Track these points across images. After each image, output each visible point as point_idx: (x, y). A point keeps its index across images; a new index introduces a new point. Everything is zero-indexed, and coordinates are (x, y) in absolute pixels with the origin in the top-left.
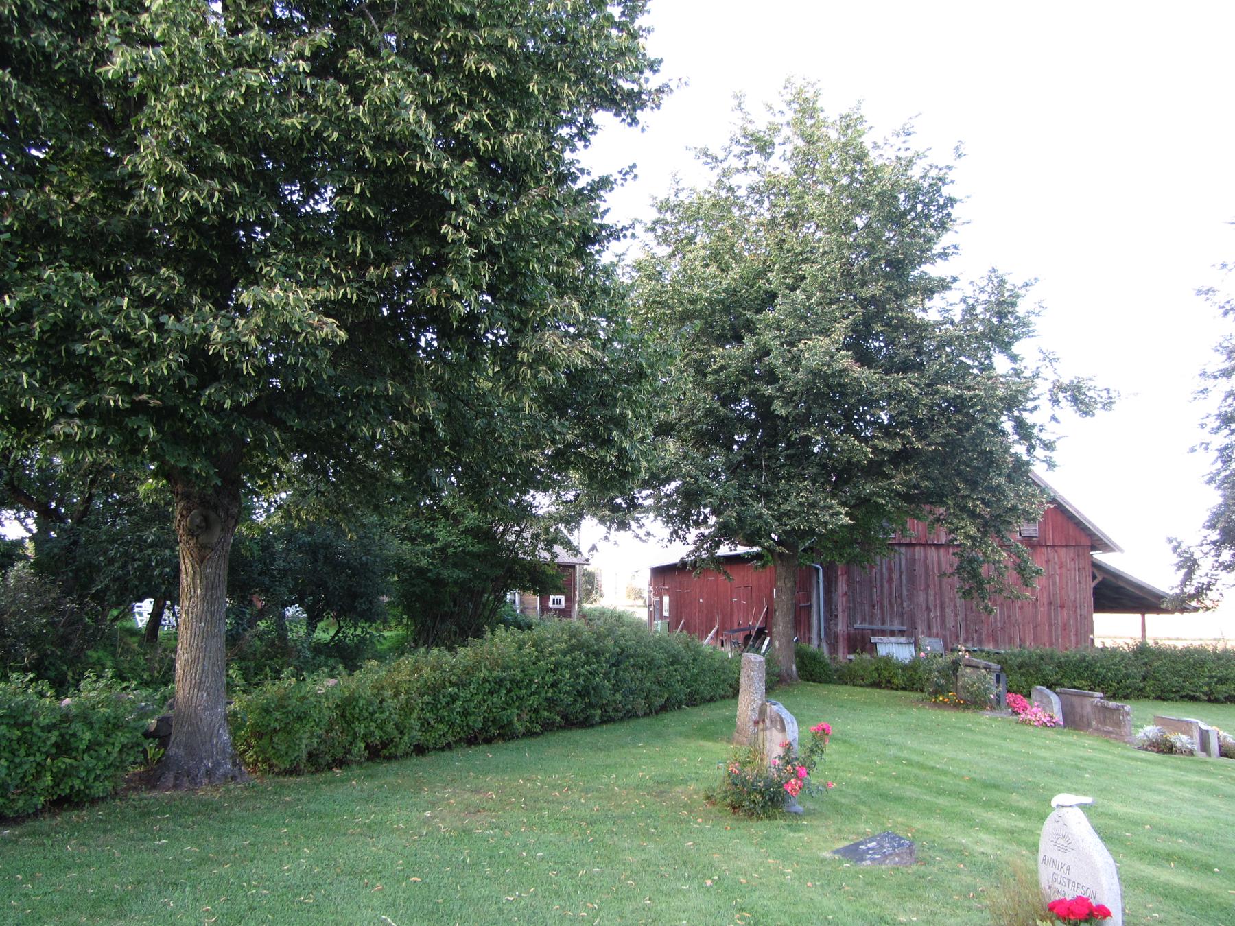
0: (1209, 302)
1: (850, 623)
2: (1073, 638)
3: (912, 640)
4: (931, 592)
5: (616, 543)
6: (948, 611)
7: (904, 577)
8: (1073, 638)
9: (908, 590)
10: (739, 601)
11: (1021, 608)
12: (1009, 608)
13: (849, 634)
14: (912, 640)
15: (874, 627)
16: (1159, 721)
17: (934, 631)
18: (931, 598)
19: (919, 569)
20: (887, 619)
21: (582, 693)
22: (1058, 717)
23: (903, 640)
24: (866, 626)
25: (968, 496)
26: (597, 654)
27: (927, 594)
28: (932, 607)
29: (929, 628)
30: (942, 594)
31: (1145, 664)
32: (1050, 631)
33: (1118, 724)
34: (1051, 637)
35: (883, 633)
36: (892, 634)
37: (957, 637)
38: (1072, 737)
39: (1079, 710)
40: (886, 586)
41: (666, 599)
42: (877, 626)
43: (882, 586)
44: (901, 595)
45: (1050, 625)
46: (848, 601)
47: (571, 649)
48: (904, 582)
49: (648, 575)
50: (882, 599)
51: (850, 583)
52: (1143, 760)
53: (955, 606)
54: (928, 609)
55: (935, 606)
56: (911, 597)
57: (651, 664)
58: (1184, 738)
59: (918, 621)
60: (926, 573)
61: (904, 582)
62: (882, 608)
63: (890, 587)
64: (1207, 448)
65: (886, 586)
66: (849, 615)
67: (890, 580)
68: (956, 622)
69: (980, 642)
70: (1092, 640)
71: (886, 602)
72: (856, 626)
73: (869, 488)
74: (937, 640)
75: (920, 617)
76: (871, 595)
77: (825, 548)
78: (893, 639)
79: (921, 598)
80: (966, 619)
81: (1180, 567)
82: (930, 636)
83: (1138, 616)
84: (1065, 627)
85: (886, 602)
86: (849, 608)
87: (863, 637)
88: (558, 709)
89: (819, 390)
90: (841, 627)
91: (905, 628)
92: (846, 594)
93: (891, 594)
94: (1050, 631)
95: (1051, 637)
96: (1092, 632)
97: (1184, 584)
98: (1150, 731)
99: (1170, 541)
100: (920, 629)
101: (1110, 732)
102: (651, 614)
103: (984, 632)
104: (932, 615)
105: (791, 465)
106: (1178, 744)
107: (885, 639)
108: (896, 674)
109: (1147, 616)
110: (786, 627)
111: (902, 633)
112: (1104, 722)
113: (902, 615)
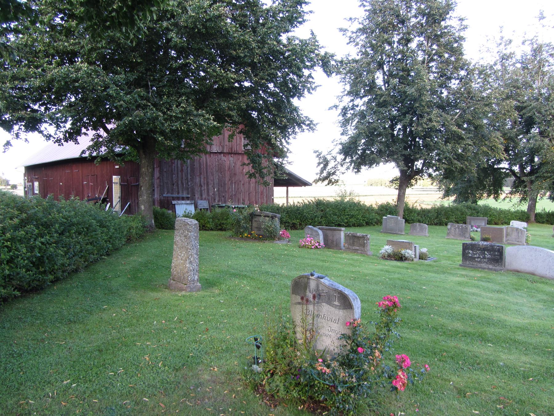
0: (345, 36)
1: (161, 194)
2: (265, 198)
3: (193, 202)
4: (202, 177)
5: (26, 140)
6: (210, 186)
7: (189, 169)
8: (265, 198)
9: (191, 176)
10: (88, 184)
11: (243, 184)
12: (238, 184)
13: (160, 200)
14: (193, 202)
15: (174, 195)
16: (389, 243)
17: (204, 197)
18: (202, 180)
19: (197, 165)
20: (181, 192)
21: (38, 263)
22: (322, 243)
23: (188, 202)
24: (170, 195)
25: (277, 115)
26: (47, 226)
27: (200, 178)
28: (202, 184)
29: (201, 195)
30: (207, 178)
31: (322, 211)
32: (256, 196)
33: (364, 245)
34: (256, 198)
35: (178, 199)
36: (183, 199)
37: (215, 199)
38: (329, 253)
39: (331, 238)
40: (180, 174)
41: (36, 184)
42: (175, 195)
43: (178, 173)
44: (187, 179)
45: (256, 193)
46: (160, 182)
47: (23, 223)
48: (189, 171)
49: (23, 170)
50: (178, 181)
51: (161, 172)
52: (403, 268)
53: (214, 184)
54: (201, 186)
55: (204, 184)
56: (192, 179)
57: (88, 230)
58: (410, 252)
59: (196, 192)
60: (200, 167)
61: (189, 171)
62: (178, 185)
63: (182, 175)
64: (336, 108)
65: (180, 174)
66: (160, 189)
67: (182, 171)
68: (214, 192)
69: (225, 202)
70: (273, 199)
71: (180, 182)
72: (164, 195)
73: (224, 105)
74: (205, 201)
75: (197, 189)
76: (172, 178)
77: (160, 150)
78: (183, 202)
79: (198, 180)
80: (218, 190)
81: (319, 164)
82: (202, 199)
83: (285, 188)
84: (262, 193)
85: (180, 182)
86: (160, 186)
87: (168, 201)
88: (14, 282)
89: (199, 30)
90: (156, 196)
91: (189, 196)
92: (159, 178)
93: (182, 178)
94: (256, 196)
95: (256, 198)
96: (273, 196)
97: (322, 172)
98: (388, 249)
99: (315, 152)
100: (197, 196)
101: (358, 250)
102: (26, 192)
103: (227, 197)
104: (203, 188)
105: (171, 86)
106: (407, 255)
107: (179, 202)
108: (209, 222)
109: (289, 188)
110: (149, 197)
111: (188, 198)
112: (353, 244)
113: (188, 189)
